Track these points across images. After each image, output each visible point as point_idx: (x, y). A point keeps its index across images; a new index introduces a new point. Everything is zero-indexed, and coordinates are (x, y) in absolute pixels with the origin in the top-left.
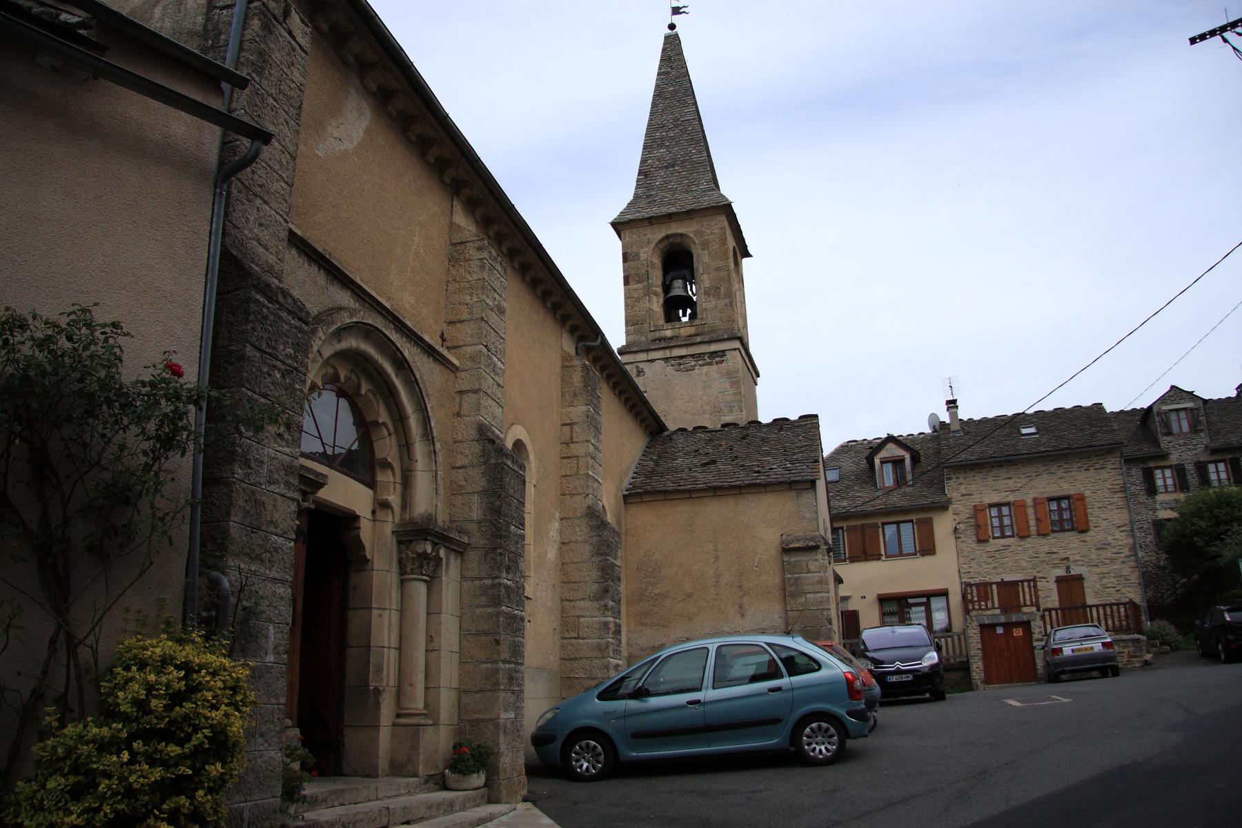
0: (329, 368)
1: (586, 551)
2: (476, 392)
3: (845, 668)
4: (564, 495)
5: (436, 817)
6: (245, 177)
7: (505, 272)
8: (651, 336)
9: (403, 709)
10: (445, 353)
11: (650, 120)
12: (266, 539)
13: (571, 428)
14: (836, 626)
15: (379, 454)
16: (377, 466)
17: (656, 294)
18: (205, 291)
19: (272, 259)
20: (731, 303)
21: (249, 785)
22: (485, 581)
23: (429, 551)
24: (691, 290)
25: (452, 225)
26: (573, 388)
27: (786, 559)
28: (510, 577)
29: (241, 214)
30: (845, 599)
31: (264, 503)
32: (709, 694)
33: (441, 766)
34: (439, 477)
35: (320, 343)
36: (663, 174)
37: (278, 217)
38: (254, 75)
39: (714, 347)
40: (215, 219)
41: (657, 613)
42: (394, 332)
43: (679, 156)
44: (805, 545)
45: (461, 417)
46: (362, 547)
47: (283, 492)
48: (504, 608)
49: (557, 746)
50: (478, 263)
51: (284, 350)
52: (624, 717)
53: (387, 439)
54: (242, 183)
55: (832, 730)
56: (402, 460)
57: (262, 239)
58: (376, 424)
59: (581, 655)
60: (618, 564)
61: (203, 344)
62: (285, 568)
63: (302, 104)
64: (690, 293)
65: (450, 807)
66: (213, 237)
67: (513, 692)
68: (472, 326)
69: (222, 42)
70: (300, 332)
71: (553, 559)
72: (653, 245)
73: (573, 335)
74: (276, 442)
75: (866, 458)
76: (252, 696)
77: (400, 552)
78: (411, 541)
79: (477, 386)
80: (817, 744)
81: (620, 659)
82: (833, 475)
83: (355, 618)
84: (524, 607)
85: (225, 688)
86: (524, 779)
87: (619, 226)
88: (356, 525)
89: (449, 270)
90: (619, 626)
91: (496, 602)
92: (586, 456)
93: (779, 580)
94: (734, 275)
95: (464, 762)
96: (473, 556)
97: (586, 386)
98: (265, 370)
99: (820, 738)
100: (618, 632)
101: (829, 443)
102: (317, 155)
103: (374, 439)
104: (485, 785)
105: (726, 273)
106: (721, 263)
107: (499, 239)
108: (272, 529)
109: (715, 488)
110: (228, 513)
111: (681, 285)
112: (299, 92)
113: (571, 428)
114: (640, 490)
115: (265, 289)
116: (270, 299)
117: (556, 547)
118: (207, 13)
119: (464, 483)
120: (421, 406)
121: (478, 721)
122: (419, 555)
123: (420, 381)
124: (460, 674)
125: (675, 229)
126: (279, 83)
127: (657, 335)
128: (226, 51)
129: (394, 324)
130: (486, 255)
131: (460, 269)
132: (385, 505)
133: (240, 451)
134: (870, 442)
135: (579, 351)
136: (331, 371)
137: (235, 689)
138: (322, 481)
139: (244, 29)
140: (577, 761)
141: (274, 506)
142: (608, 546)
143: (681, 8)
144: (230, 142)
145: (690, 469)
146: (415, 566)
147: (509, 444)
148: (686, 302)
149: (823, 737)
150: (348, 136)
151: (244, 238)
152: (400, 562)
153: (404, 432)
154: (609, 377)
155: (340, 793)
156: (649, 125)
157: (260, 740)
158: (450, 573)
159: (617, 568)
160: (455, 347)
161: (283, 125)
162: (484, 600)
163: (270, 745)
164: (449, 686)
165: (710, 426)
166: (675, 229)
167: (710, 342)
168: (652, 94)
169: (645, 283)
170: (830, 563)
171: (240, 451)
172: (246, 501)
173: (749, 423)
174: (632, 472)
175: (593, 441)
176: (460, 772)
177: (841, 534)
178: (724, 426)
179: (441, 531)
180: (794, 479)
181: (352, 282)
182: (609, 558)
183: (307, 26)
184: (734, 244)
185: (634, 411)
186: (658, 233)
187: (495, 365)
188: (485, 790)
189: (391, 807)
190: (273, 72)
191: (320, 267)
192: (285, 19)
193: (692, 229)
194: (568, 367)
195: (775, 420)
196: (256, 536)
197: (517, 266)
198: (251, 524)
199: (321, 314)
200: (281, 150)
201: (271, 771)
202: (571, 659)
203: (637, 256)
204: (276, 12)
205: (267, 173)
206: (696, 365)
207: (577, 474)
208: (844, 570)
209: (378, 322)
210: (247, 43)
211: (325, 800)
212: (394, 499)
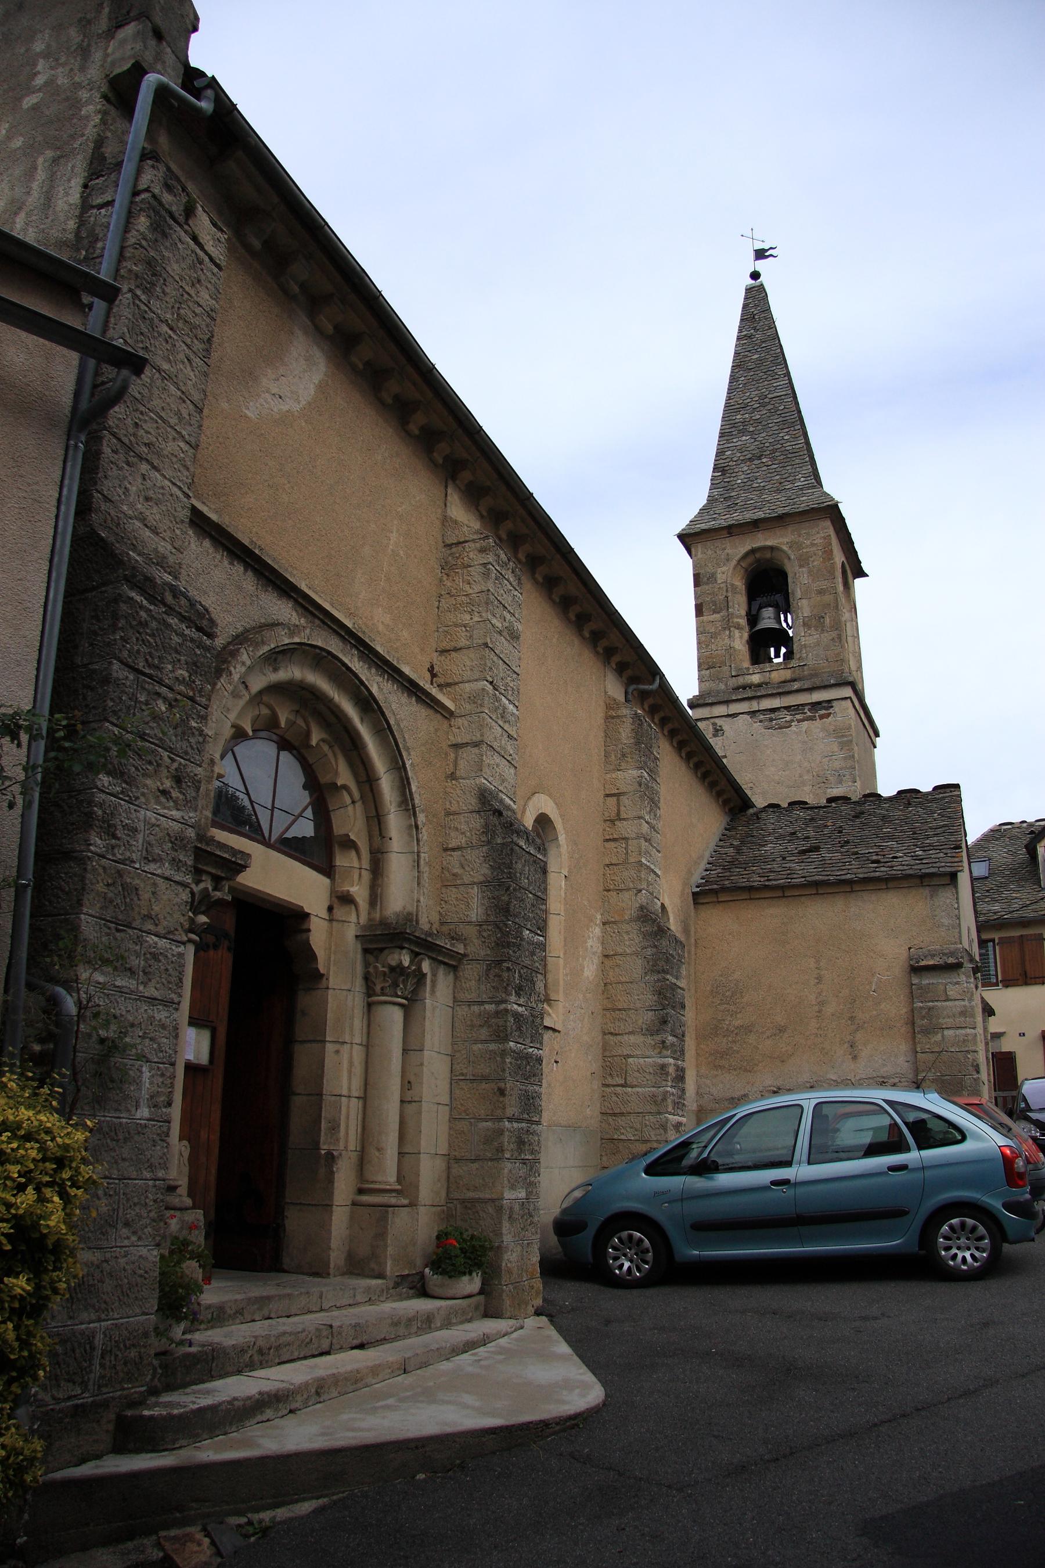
0: (262, 707)
1: (636, 967)
2: (476, 744)
3: (1001, 1140)
4: (609, 890)
5: (404, 1337)
6: (122, 431)
7: (520, 583)
8: (733, 682)
9: (368, 1182)
10: (434, 691)
11: (729, 398)
12: (139, 941)
13: (618, 800)
14: (985, 1075)
15: (338, 829)
16: (336, 846)
17: (738, 627)
18: (49, 583)
19: (164, 548)
20: (839, 637)
21: (105, 1297)
22: (487, 1006)
23: (406, 963)
24: (786, 620)
25: (445, 520)
26: (620, 746)
27: (915, 981)
28: (521, 1001)
29: (117, 482)
30: (997, 1036)
31: (137, 889)
32: (801, 1171)
33: (419, 1262)
34: (422, 862)
35: (243, 669)
36: (746, 468)
37: (175, 490)
38: (139, 292)
39: (817, 697)
40: (66, 482)
41: (738, 1052)
42: (356, 659)
43: (767, 445)
44: (941, 962)
45: (456, 779)
46: (313, 957)
47: (167, 873)
48: (511, 1044)
49: (587, 1236)
50: (481, 569)
51: (173, 671)
52: (682, 1200)
53: (350, 808)
54: (119, 440)
55: (982, 1230)
56: (371, 837)
57: (150, 518)
58: (335, 788)
59: (629, 1110)
60: (682, 985)
61: (43, 657)
62: (169, 982)
63: (213, 336)
64: (784, 625)
65: (427, 1323)
66: (63, 508)
67: (524, 1162)
68: (472, 656)
69: (98, 252)
70: (198, 647)
71: (591, 979)
72: (734, 562)
73: (621, 677)
74: (159, 803)
75: (1026, 847)
76: (86, 1171)
77: (366, 964)
78: (382, 950)
79: (478, 738)
80: (959, 1248)
81: (683, 1116)
82: (980, 869)
83: (302, 1055)
84: (541, 1043)
85: (44, 1160)
86: (538, 1283)
87: (688, 539)
88: (305, 927)
89: (441, 581)
90: (683, 1070)
91: (500, 1035)
92: (638, 838)
93: (905, 1010)
94: (843, 599)
95: (450, 1258)
96: (470, 972)
97: (638, 743)
98: (143, 699)
99: (963, 1241)
100: (680, 1078)
101: (976, 827)
102: (246, 417)
103: (331, 809)
104: (481, 1293)
105: (832, 597)
106: (824, 584)
107: (514, 542)
108: (149, 926)
109: (817, 884)
110: (80, 903)
111: (772, 616)
112: (208, 320)
113: (618, 800)
114: (715, 886)
115: (146, 585)
116: (152, 599)
117: (596, 961)
118: (80, 216)
119: (459, 871)
120: (397, 763)
121: (474, 1201)
122: (392, 969)
123: (395, 728)
124: (450, 1135)
125: (763, 540)
126: (177, 305)
127: (741, 681)
128: (101, 263)
129: (358, 649)
130: (490, 558)
131: (456, 578)
132: (347, 899)
133: (100, 812)
134: (1031, 825)
135: (630, 697)
136: (265, 711)
137: (61, 1163)
138: (242, 863)
139: (126, 230)
140: (616, 1259)
141: (154, 893)
142: (667, 961)
143: (767, 250)
144: (103, 383)
145: (784, 859)
146: (387, 985)
147: (529, 821)
148: (780, 638)
149: (968, 1239)
150: (292, 392)
151: (122, 516)
152: (366, 978)
153: (375, 801)
154: (672, 734)
155: (263, 1301)
156: (727, 406)
157: (125, 1232)
158: (438, 994)
159: (679, 990)
160: (449, 685)
161: (183, 363)
162: (484, 1033)
163: (140, 1238)
164: (433, 1152)
165: (810, 800)
166: (763, 540)
167: (811, 690)
168: (731, 365)
169: (724, 613)
170: (977, 987)
171: (100, 812)
172: (108, 885)
173: (865, 796)
174: (705, 861)
175: (647, 817)
176: (444, 1273)
177: (991, 949)
178: (830, 800)
179: (423, 936)
180: (927, 871)
181: (295, 588)
182: (668, 977)
183: (222, 231)
184: (843, 559)
185: (707, 780)
186: (740, 547)
187: (505, 708)
188: (482, 1298)
189: (336, 1324)
190: (167, 290)
191: (247, 566)
192: (187, 220)
193: (786, 540)
194: (613, 717)
195: (900, 792)
196: (122, 934)
197: (540, 579)
198: (116, 918)
199: (248, 631)
200: (181, 398)
201: (141, 1276)
202: (614, 1114)
203: (712, 578)
204: (174, 208)
205: (158, 428)
206: (793, 721)
207: (626, 862)
208: (997, 997)
209: (334, 645)
210: (130, 250)
211: (240, 1312)
212: (359, 890)
